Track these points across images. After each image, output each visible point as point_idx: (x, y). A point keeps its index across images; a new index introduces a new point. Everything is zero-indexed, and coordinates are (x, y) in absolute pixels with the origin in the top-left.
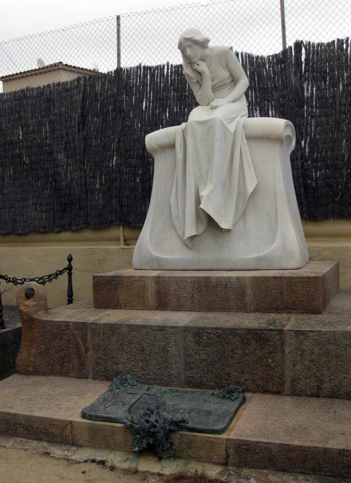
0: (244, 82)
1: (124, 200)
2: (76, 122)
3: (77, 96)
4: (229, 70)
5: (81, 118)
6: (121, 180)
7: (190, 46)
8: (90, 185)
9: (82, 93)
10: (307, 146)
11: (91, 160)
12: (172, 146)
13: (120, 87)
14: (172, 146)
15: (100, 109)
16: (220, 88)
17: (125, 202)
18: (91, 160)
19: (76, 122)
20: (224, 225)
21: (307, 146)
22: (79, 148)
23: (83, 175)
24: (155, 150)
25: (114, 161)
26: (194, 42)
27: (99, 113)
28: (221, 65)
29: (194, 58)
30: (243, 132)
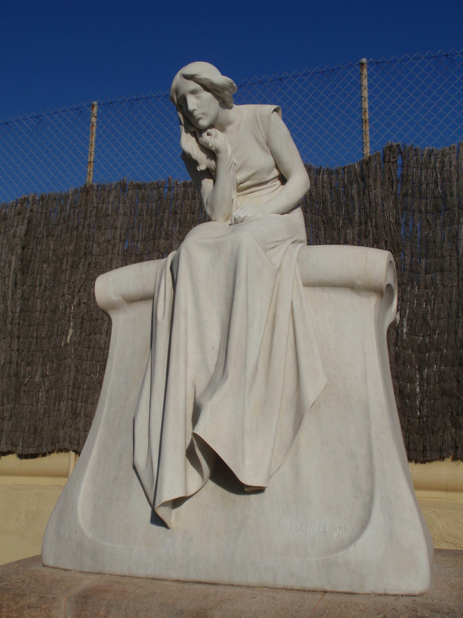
0: (299, 183)
1: (79, 405)
2: (13, 268)
3: (17, 226)
4: (273, 154)
5: (20, 263)
6: (77, 371)
7: (194, 92)
8: (24, 377)
9: (26, 222)
10: (405, 323)
11: (30, 333)
12: (150, 298)
13: (89, 214)
14: (150, 298)
15: (54, 250)
16: (253, 189)
17: (81, 408)
18: (30, 333)
19: (13, 268)
20: (247, 478)
21: (405, 323)
22: (12, 312)
23: (15, 359)
24: (115, 306)
25: (69, 337)
26: (202, 85)
27: (51, 255)
28: (257, 140)
29: (200, 119)
30: (297, 269)
